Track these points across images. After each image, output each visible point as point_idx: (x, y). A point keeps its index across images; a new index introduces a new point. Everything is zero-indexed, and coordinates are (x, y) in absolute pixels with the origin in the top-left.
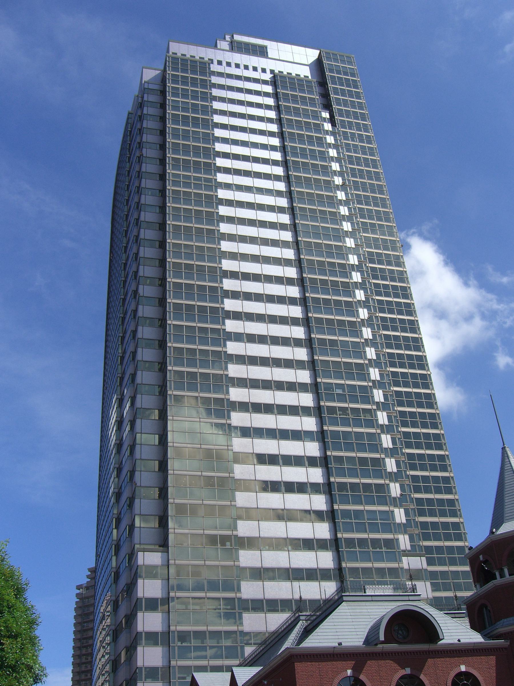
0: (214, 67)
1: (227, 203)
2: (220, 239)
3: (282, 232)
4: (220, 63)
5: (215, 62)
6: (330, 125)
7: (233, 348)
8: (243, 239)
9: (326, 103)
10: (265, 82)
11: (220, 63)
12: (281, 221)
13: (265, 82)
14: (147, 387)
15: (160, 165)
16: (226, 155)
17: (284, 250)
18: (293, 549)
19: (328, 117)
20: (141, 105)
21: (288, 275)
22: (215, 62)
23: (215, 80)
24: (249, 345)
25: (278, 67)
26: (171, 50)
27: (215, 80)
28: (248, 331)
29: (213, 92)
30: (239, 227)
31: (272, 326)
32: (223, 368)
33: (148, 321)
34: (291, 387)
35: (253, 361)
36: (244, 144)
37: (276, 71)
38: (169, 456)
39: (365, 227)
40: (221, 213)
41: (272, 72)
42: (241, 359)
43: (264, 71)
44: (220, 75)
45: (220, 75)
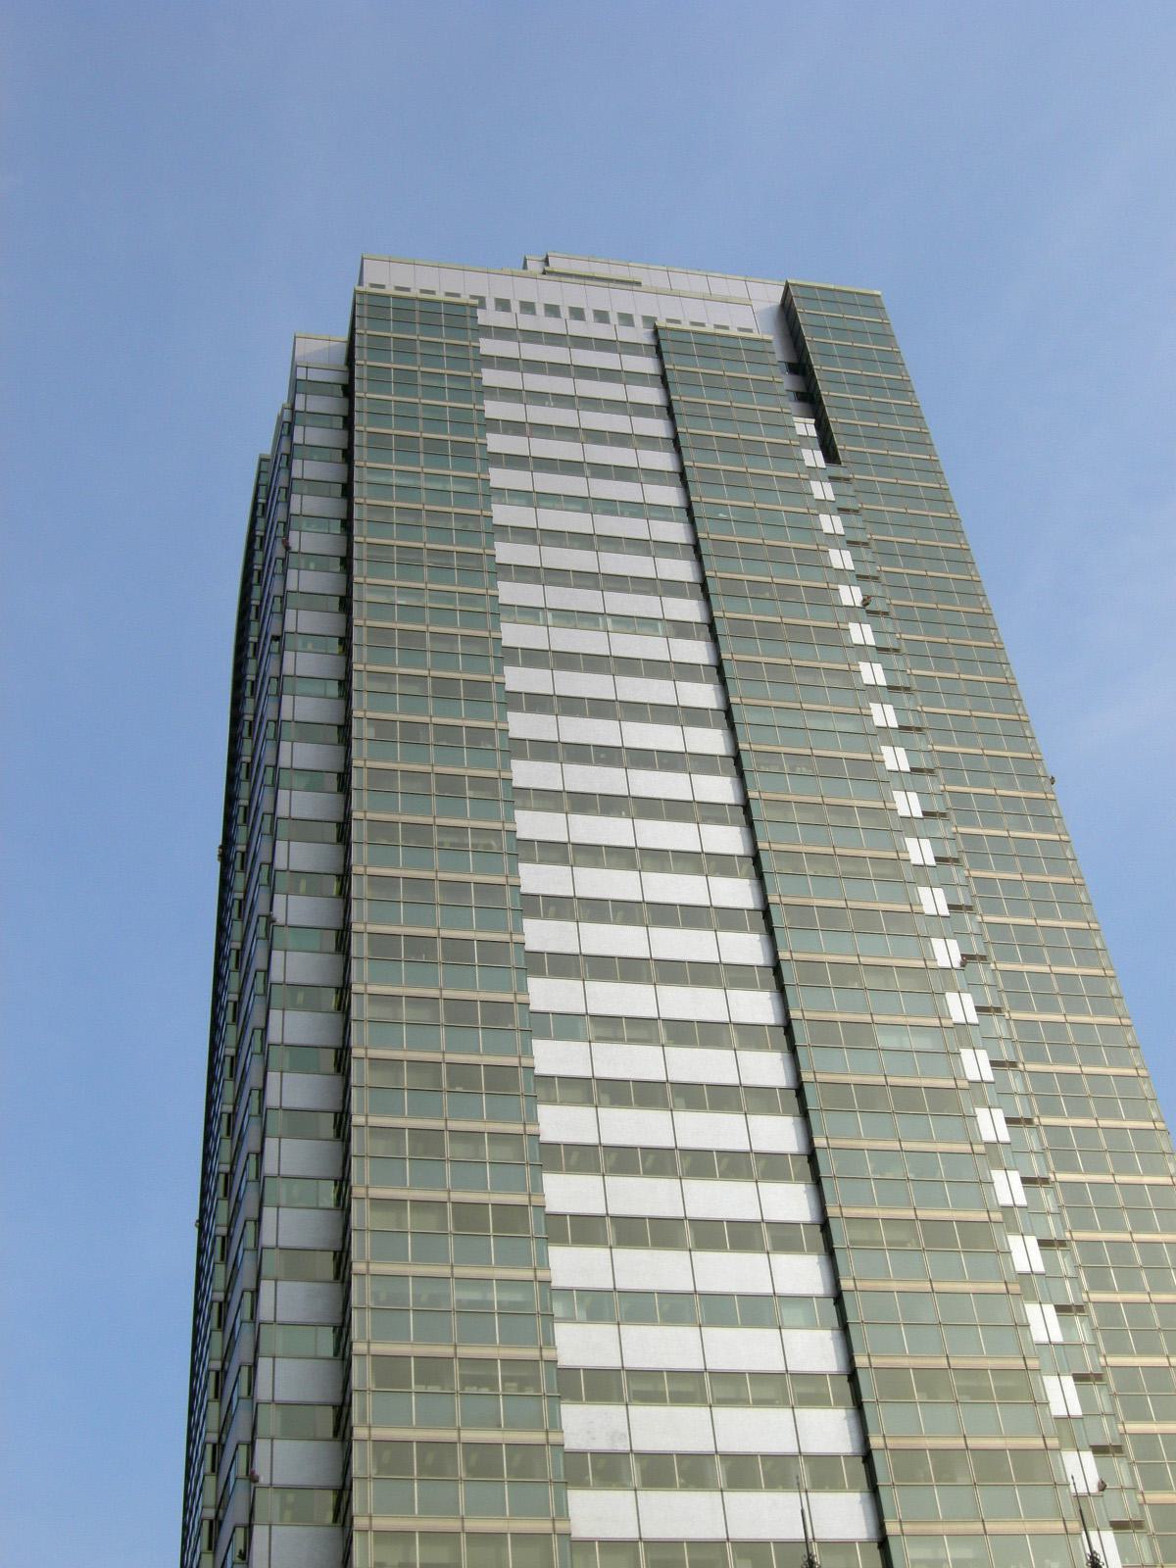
0: (488, 317)
1: (552, 909)
2: (529, 1033)
3: (728, 938)
4: (503, 305)
5: (490, 304)
6: (819, 454)
7: (541, 935)
8: (597, 910)
9: (794, 360)
10: (631, 348)
11: (503, 305)
12: (761, 1145)
13: (631, 348)
14: (297, 1186)
15: (341, 572)
16: (544, 750)
17: (736, 995)
18: (632, 764)
19: (813, 432)
20: (287, 427)
21: (743, 1015)
22: (490, 304)
23: (488, 346)
24: (623, 1255)
25: (666, 312)
26: (368, 279)
27: (488, 346)
28: (568, 737)
29: (491, 477)
30: (564, 720)
31: (660, 934)
32: (519, 1049)
33: (303, 885)
34: (736, 1165)
35: (632, 1231)
36: (658, 1162)
37: (661, 323)
38: (353, 735)
39: (1031, 1040)
40: (532, 945)
41: (649, 320)
42: (563, 965)
43: (627, 319)
44: (503, 333)
45: (503, 333)
